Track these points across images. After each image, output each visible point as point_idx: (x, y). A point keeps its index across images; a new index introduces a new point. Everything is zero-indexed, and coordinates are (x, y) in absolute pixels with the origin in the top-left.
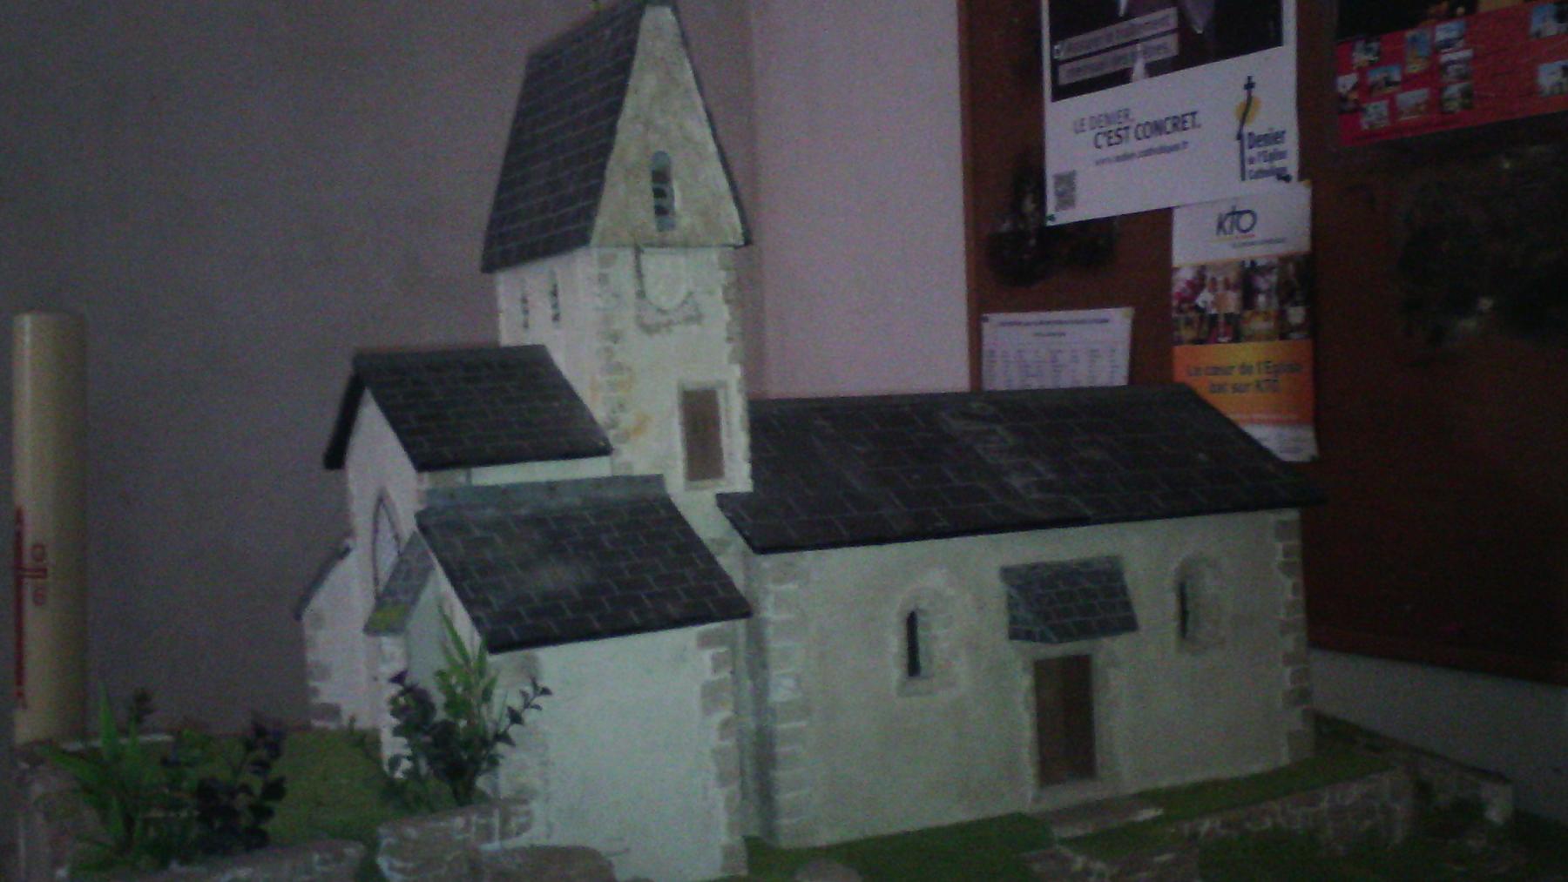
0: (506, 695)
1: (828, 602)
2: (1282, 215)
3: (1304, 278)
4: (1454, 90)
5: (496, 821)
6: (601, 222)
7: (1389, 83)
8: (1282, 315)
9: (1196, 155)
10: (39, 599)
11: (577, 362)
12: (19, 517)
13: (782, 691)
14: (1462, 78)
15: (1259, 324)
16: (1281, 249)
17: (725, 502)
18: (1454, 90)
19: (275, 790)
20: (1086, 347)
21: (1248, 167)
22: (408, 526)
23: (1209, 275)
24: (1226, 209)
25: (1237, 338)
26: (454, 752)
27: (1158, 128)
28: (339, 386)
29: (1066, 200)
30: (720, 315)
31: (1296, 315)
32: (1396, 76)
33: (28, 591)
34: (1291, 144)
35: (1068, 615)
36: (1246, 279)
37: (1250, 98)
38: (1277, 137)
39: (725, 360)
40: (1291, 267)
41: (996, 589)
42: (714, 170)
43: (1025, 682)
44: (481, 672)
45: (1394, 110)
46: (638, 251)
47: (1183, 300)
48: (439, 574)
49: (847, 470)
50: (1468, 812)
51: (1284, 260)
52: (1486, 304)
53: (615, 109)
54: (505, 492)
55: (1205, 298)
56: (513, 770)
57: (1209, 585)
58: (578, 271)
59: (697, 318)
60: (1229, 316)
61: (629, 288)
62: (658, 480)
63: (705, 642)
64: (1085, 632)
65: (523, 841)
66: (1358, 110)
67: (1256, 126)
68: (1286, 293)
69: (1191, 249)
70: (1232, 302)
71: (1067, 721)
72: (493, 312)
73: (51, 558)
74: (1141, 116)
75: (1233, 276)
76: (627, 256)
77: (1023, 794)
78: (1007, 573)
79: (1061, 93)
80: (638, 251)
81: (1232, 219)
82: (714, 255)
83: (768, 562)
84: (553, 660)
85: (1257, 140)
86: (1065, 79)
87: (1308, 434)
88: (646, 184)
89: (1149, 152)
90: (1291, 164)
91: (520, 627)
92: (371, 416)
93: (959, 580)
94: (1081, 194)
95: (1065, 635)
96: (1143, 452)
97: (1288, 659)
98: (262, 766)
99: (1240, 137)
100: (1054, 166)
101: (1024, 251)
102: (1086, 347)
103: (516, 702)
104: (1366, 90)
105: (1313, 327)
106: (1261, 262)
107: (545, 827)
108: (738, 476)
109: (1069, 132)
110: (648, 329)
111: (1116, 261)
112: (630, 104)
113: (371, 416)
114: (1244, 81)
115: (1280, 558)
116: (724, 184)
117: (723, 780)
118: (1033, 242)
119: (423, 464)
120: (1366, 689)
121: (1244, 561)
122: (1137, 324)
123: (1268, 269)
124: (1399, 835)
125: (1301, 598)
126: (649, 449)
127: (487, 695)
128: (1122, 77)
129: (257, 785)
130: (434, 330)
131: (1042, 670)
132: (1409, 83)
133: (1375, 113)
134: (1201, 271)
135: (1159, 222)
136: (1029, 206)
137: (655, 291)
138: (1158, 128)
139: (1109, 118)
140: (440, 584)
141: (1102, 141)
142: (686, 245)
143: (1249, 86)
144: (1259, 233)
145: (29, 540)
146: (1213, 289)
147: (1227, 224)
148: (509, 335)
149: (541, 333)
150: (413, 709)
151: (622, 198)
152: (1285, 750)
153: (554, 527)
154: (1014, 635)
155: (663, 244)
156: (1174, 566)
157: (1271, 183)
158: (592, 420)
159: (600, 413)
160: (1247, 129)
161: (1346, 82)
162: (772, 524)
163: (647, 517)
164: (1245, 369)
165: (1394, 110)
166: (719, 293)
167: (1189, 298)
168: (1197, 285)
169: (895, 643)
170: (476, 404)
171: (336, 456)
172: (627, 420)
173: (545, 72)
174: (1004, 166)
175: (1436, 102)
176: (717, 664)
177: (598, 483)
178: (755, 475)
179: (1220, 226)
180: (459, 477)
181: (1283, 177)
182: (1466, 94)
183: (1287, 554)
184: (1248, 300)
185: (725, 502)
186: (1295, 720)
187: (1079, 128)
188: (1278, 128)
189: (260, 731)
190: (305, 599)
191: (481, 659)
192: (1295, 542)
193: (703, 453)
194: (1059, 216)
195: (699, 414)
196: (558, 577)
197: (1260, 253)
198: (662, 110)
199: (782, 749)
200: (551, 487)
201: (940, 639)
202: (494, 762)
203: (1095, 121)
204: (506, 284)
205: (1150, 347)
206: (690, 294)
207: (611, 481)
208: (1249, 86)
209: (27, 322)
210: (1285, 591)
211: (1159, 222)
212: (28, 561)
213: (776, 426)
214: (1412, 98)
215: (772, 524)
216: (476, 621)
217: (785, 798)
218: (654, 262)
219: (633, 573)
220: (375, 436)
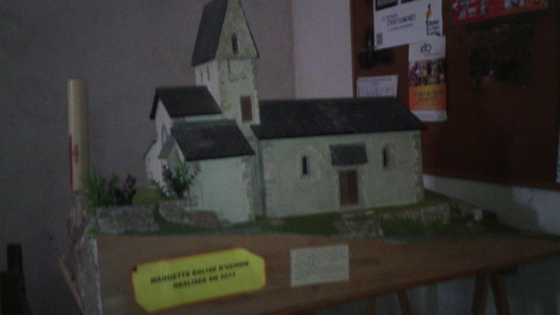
0: (191, 172)
1: (282, 155)
2: (438, 46)
3: (445, 65)
4: (483, 8)
5: (188, 203)
6: (218, 53)
7: (466, 5)
8: (438, 77)
9: (415, 29)
10: (77, 161)
11: (214, 90)
12: (70, 138)
13: (267, 176)
14: (485, 4)
15: (432, 80)
16: (437, 57)
17: (254, 128)
18: (483, 8)
19: (134, 192)
20: (386, 86)
21: (429, 31)
22: (169, 132)
23: (418, 65)
24: (423, 45)
25: (426, 84)
26: (179, 186)
27: (405, 19)
28: (153, 96)
29: (380, 42)
30: (251, 77)
31: (442, 76)
32: (468, 3)
33: (73, 158)
34: (441, 24)
35: (348, 159)
36: (429, 66)
37: (429, 10)
38: (436, 22)
39: (252, 88)
40: (441, 62)
41: (328, 152)
42: (249, 39)
43: (336, 177)
44: (185, 165)
45: (467, 14)
46: (229, 60)
47: (411, 72)
48: (176, 143)
49: (289, 118)
50: (470, 217)
51: (439, 60)
52: (491, 72)
53: (222, 22)
54: (193, 124)
55: (417, 72)
56: (193, 191)
57: (392, 151)
58: (213, 65)
59: (245, 77)
60: (424, 78)
61: (226, 70)
62: (234, 121)
63: (243, 161)
64: (352, 163)
65: (195, 209)
66: (458, 14)
67: (431, 19)
68: (439, 70)
69: (414, 57)
70: (425, 72)
71: (350, 188)
72: (195, 77)
73: (80, 150)
74: (400, 16)
75: (425, 65)
76: (226, 61)
77: (336, 206)
78: (331, 147)
79: (379, 8)
80: (229, 60)
81: (425, 48)
82: (249, 61)
83: (264, 142)
84: (204, 165)
85: (431, 23)
86: (379, 4)
87: (445, 113)
88: (230, 42)
89: (402, 27)
90: (441, 30)
91: (195, 156)
92: (161, 107)
93: (318, 149)
94: (384, 40)
95: (346, 164)
96: (388, 116)
97: (416, 173)
98: (131, 187)
99: (427, 22)
100: (377, 31)
101: (369, 58)
102: (386, 86)
103: (193, 174)
104: (460, 8)
105: (446, 80)
106: (432, 60)
107: (202, 205)
108: (256, 120)
109: (380, 20)
110: (231, 81)
111: (391, 60)
112: (226, 21)
113: (161, 107)
114: (427, 6)
115: (414, 144)
116: (252, 42)
117: (248, 196)
118: (371, 55)
119: (172, 115)
120: (456, 188)
121: (406, 146)
122: (399, 81)
123: (434, 63)
124: (445, 221)
125: (421, 156)
126: (232, 112)
127: (187, 172)
128: (395, 4)
129: (130, 191)
130: (182, 82)
131: (341, 174)
132: (471, 6)
133: (462, 15)
134: (417, 64)
135: (405, 49)
136: (370, 44)
137: (234, 71)
138: (405, 19)
139: (392, 16)
140: (177, 147)
141: (390, 24)
142: (242, 58)
143: (429, 6)
144: (432, 51)
145: (73, 144)
146: (420, 68)
147: (424, 49)
148: (198, 83)
149: (206, 83)
150: (167, 175)
151: (224, 46)
152: (415, 199)
153: (206, 132)
154: (333, 163)
155: (235, 58)
156: (381, 146)
157: (435, 37)
158: (216, 104)
159: (219, 102)
160: (429, 19)
161: (455, 5)
162: (264, 133)
163: (231, 130)
164: (428, 93)
165: (467, 14)
166: (251, 71)
167: (413, 72)
168: (416, 68)
169: (299, 165)
170: (186, 101)
171: (153, 116)
172: (226, 105)
173: (207, 11)
174: (363, 32)
175: (478, 11)
176: (246, 167)
177: (218, 122)
178: (261, 119)
179: (422, 49)
180: (181, 120)
181: (438, 34)
182: (486, 9)
183: (416, 143)
184: (429, 72)
185: (254, 128)
186: (419, 190)
187: (383, 20)
188: (437, 19)
189: (130, 177)
190: (145, 155)
191: (185, 163)
192: (419, 140)
193: (247, 114)
194: (378, 47)
195: (246, 103)
196: (206, 144)
197: (432, 58)
198: (234, 23)
199: (267, 192)
200: (206, 123)
201: (313, 165)
202: (188, 189)
203: (388, 17)
204: (198, 70)
205: (403, 87)
206: (242, 72)
207: (222, 121)
208: (429, 6)
209: (71, 84)
210: (416, 154)
211: (405, 49)
212: (73, 150)
213: (267, 108)
214: (472, 10)
215: (264, 133)
216: (184, 154)
217: (268, 204)
218: (233, 63)
219: (226, 143)
220: (162, 110)
